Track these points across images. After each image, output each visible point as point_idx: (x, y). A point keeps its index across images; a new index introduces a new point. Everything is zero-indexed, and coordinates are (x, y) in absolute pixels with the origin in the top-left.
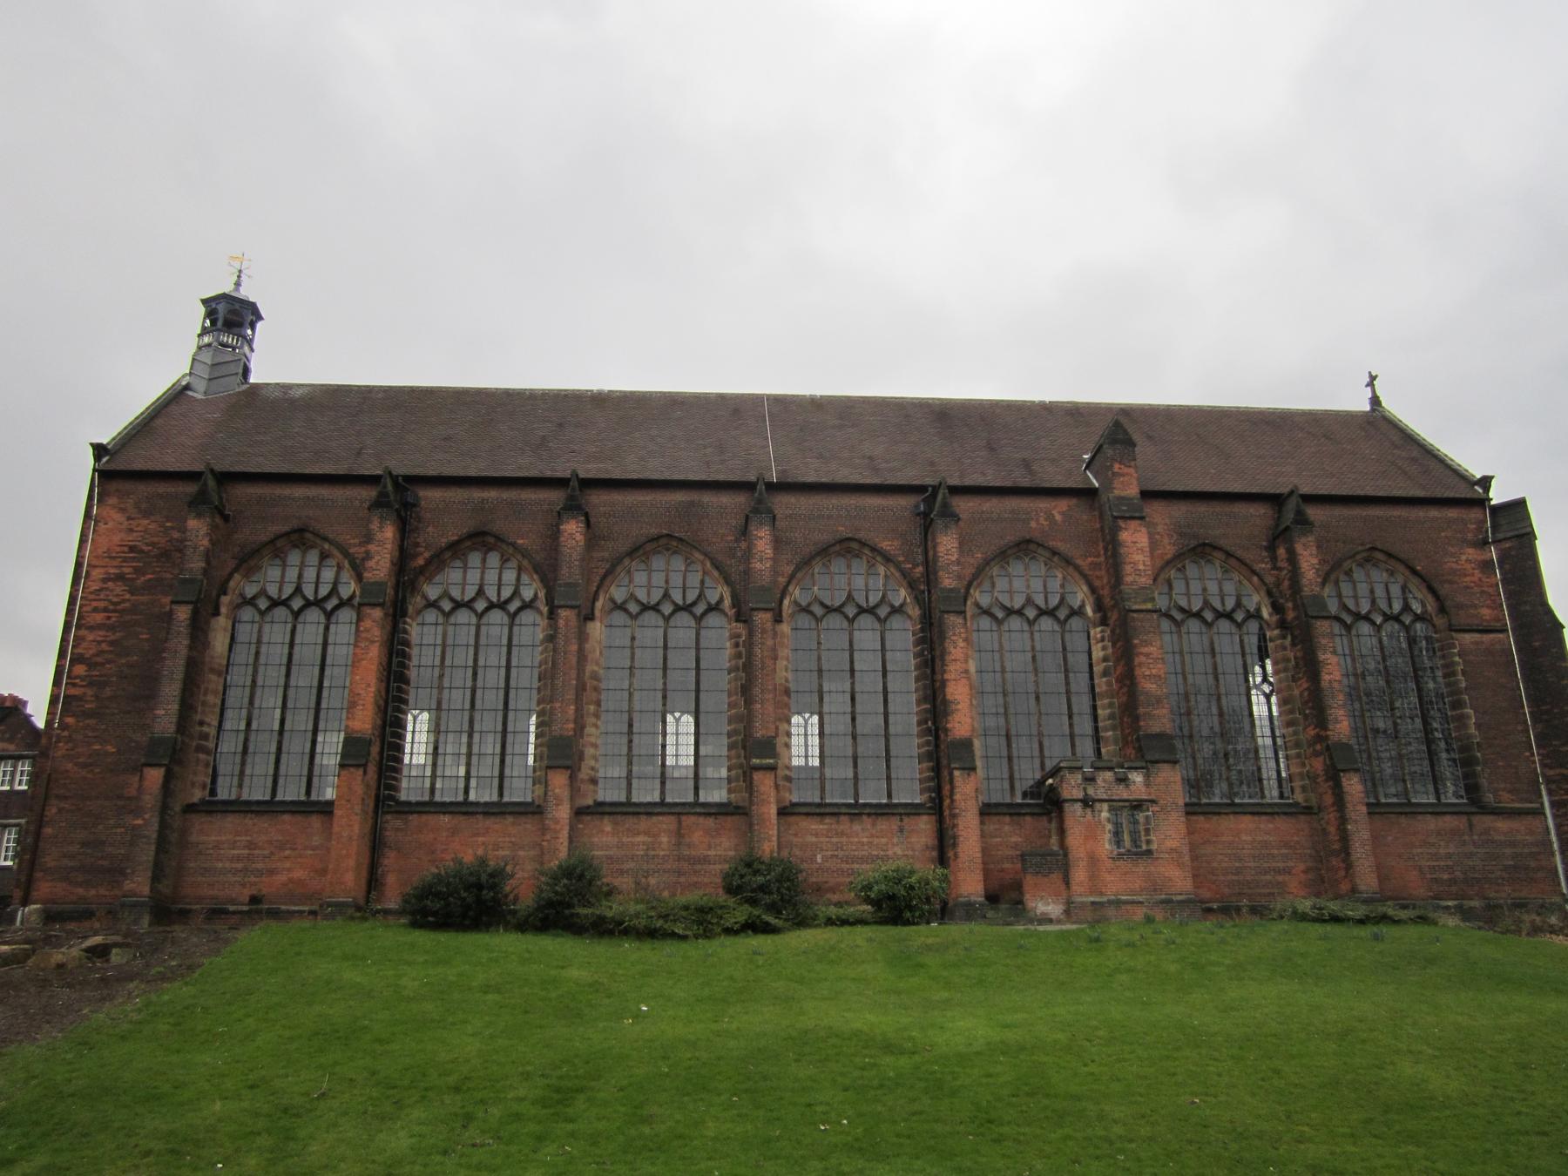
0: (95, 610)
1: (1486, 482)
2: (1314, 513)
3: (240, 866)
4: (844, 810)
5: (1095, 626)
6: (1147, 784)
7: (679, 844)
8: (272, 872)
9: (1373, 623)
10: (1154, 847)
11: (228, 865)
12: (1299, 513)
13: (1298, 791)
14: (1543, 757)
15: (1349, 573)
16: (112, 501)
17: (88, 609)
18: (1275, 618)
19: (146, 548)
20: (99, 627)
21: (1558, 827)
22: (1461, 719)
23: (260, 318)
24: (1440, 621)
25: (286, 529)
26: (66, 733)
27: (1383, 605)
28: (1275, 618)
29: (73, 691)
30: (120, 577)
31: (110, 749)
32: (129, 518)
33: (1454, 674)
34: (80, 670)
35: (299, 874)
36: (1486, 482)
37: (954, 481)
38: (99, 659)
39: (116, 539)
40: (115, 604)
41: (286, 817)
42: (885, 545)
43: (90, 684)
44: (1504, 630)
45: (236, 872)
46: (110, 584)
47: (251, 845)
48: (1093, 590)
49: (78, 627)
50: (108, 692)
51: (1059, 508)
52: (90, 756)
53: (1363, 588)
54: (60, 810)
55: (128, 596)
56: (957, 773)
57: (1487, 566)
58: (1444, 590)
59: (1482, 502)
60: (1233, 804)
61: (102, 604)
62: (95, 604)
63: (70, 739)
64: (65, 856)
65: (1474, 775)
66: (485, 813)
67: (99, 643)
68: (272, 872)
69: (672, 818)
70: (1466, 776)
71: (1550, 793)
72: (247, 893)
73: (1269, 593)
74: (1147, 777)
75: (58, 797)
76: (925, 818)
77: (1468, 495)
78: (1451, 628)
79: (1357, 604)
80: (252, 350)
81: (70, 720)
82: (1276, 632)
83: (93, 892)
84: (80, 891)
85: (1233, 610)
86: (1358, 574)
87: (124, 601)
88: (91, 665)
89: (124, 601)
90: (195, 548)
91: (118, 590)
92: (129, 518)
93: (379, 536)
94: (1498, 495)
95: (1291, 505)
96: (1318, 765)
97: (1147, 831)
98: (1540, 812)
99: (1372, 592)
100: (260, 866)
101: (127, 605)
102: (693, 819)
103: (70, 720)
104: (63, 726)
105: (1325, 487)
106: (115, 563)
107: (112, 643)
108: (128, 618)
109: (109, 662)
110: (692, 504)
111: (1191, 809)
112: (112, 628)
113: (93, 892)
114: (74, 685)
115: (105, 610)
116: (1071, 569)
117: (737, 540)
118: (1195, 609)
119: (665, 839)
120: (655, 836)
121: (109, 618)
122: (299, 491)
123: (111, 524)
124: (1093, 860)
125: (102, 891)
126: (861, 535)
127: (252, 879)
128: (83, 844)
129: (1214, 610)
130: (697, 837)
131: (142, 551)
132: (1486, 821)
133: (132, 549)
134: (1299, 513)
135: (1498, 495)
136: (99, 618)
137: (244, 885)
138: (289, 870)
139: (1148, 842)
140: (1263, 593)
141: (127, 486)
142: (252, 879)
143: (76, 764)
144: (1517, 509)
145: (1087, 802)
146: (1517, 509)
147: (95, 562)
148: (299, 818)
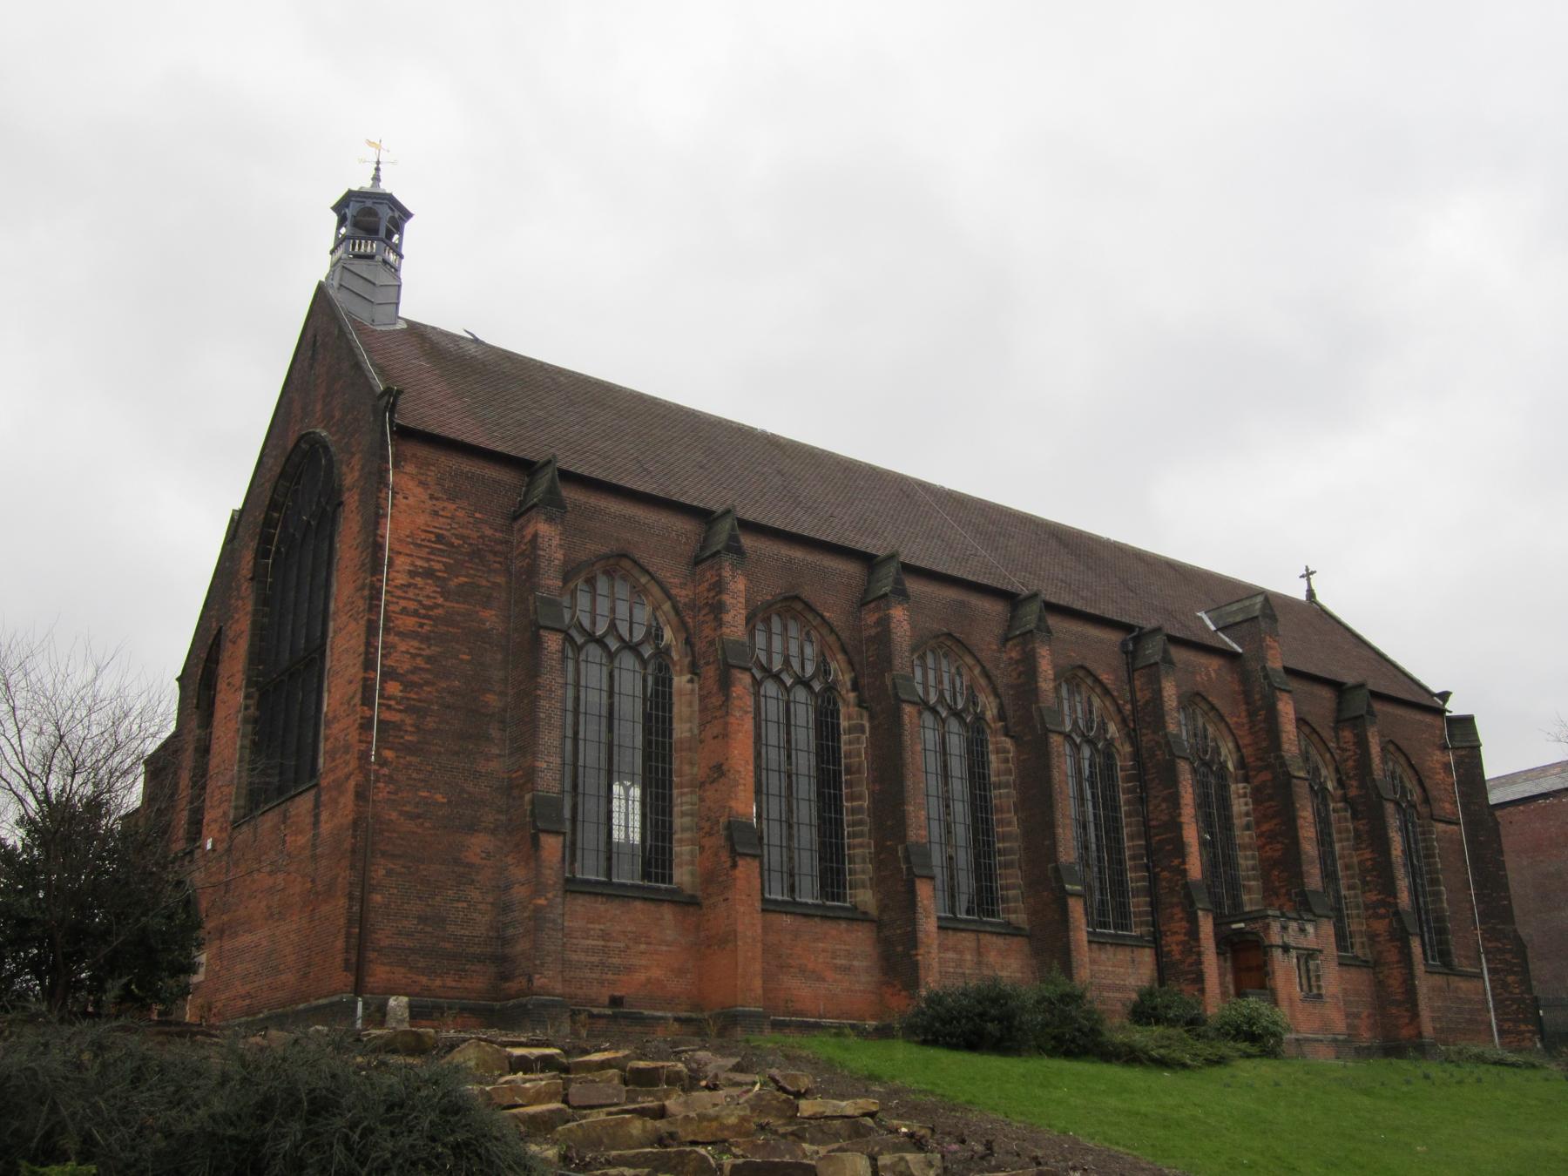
0: (404, 611)
1: (1445, 696)
2: (914, 586)
3: (595, 959)
4: (843, 914)
5: (1237, 782)
6: (1317, 936)
7: (979, 963)
8: (630, 969)
9: (782, 682)
10: (1323, 991)
11: (582, 957)
12: (733, 538)
13: (1357, 946)
14: (1484, 932)
15: (591, 582)
16: (410, 468)
17: (397, 609)
18: (1340, 792)
19: (457, 542)
20: (413, 635)
21: (1493, 989)
22: (1438, 894)
23: (407, 215)
24: (1423, 809)
25: (605, 550)
26: (385, 771)
27: (623, 629)
28: (1340, 792)
29: (387, 716)
30: (429, 574)
31: (439, 798)
32: (432, 497)
33: (1433, 856)
34: (394, 688)
35: (656, 973)
36: (1445, 696)
37: (749, 516)
38: (415, 678)
39: (422, 520)
40: (425, 607)
41: (638, 904)
42: (1104, 677)
43: (408, 710)
44: (1458, 824)
45: (593, 967)
46: (419, 581)
47: (605, 936)
48: (1238, 748)
49: (387, 630)
50: (430, 723)
51: (1214, 664)
52: (417, 805)
53: (603, 606)
54: (389, 873)
55: (440, 600)
56: (1200, 913)
57: (1447, 766)
58: (1428, 783)
59: (1441, 712)
60: (795, 903)
61: (412, 606)
62: (403, 603)
63: (390, 779)
64: (400, 933)
65: (1447, 942)
66: (823, 917)
67: (414, 656)
68: (630, 969)
69: (972, 936)
70: (1440, 943)
71: (1488, 961)
72: (605, 994)
73: (1337, 770)
74: (1316, 929)
75: (384, 854)
76: (1147, 951)
77: (1429, 705)
78: (1432, 817)
79: (594, 623)
80: (401, 257)
81: (389, 754)
82: (1341, 805)
83: (438, 982)
84: (424, 980)
85: (641, 643)
86: (602, 585)
87: (437, 606)
88: (408, 686)
89: (437, 606)
90: (550, 561)
91: (429, 590)
92: (432, 497)
93: (732, 586)
94: (1454, 708)
95: (725, 527)
96: (1380, 926)
97: (1318, 977)
98: (1480, 976)
99: (613, 610)
100: (616, 961)
101: (440, 611)
102: (988, 937)
103: (389, 754)
104: (383, 762)
105: (1065, 599)
106: (424, 553)
107: (429, 659)
108: (443, 629)
109: (427, 683)
110: (963, 604)
111: (944, 924)
112: (425, 639)
113: (438, 982)
114: (389, 707)
115: (416, 613)
116: (1222, 726)
117: (999, 651)
118: (599, 633)
119: (968, 957)
120: (961, 952)
121: (421, 625)
122: (614, 506)
123: (411, 500)
124: (1291, 1000)
125: (450, 982)
126: (1087, 664)
127: (610, 976)
128: (422, 919)
129: (621, 639)
130: (992, 957)
131: (452, 545)
132: (1456, 982)
133: (440, 538)
134: (733, 538)
135: (1454, 708)
136: (410, 622)
137: (602, 983)
138: (646, 968)
139: (1319, 987)
140: (1331, 768)
141: (424, 452)
142: (610, 976)
143: (401, 813)
144: (1467, 722)
145: (1286, 949)
146: (1467, 722)
147: (397, 547)
148: (652, 907)
